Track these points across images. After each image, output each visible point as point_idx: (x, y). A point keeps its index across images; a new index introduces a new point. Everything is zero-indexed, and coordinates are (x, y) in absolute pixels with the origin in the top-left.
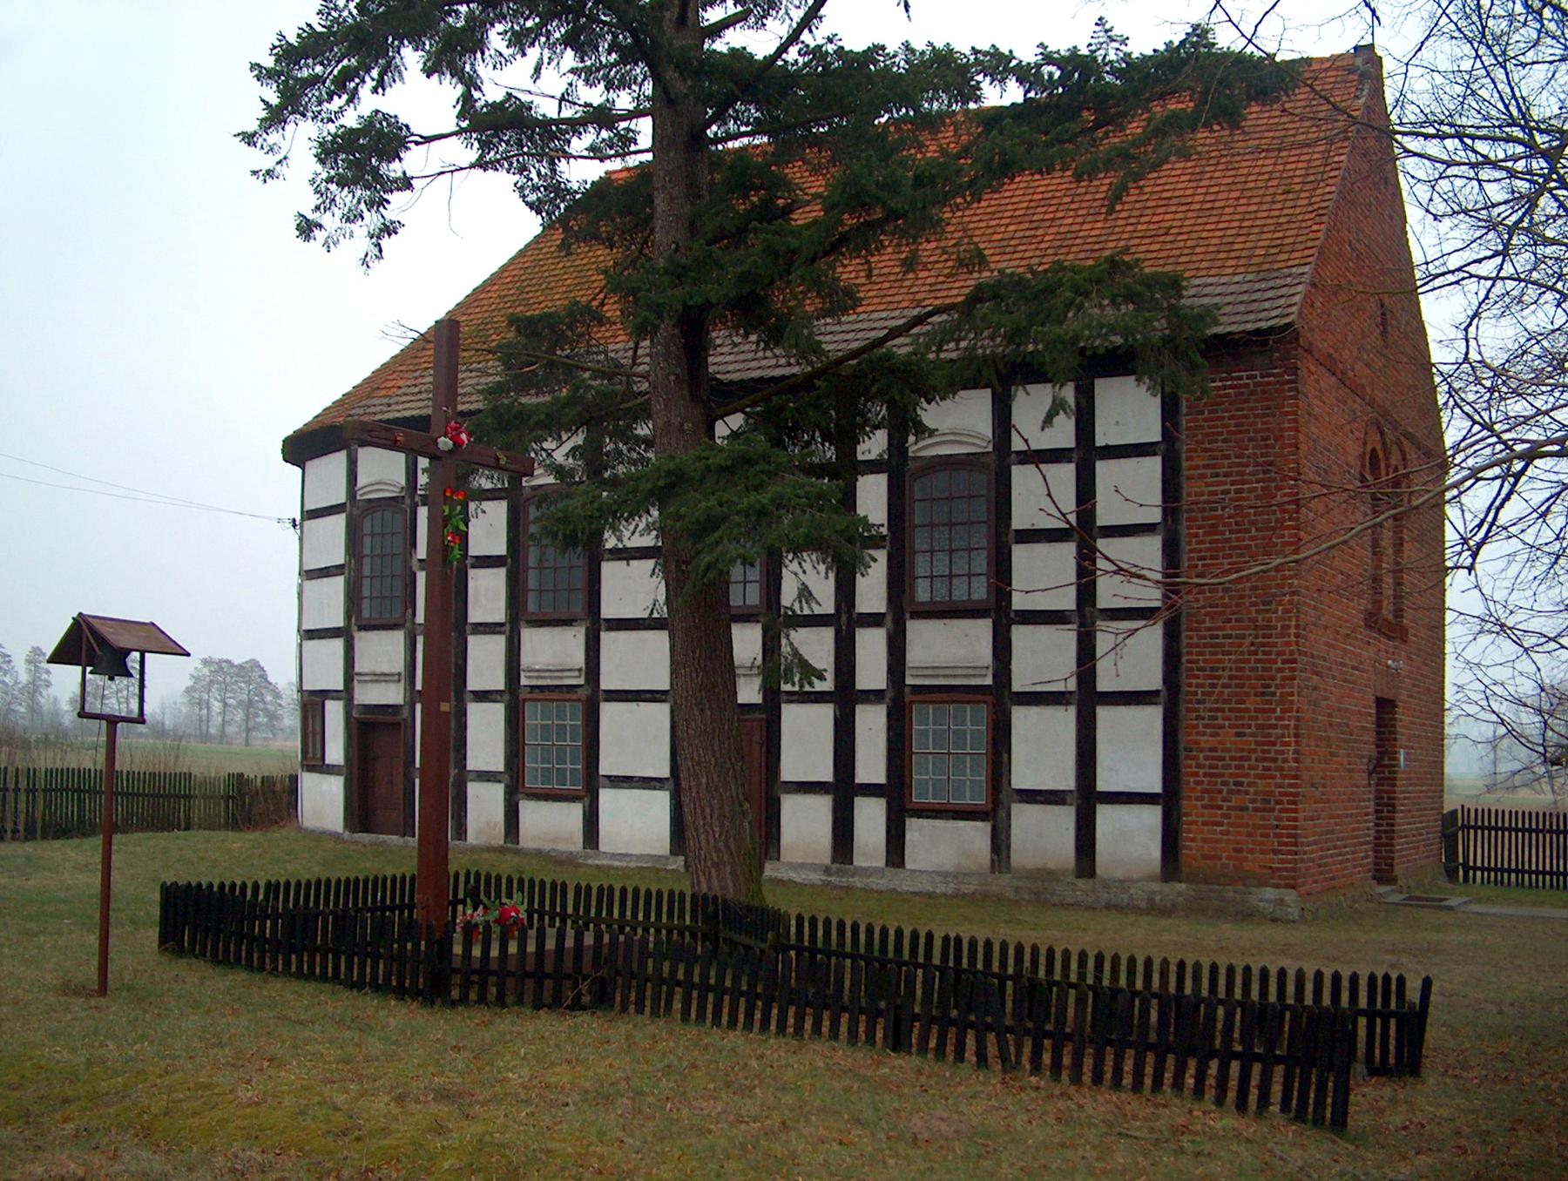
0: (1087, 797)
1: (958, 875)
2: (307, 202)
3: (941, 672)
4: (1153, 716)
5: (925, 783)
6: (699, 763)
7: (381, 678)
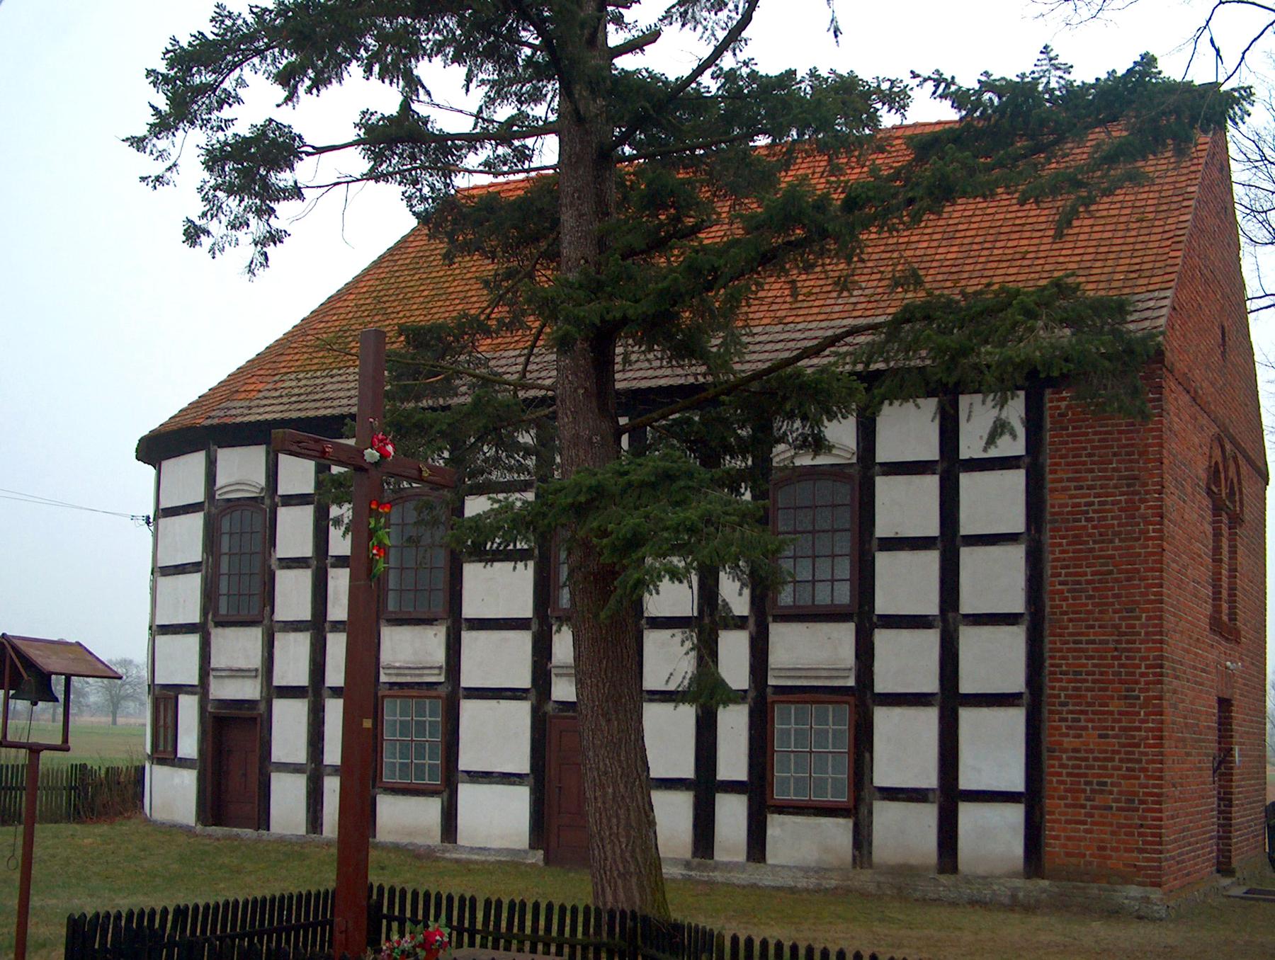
0: (949, 796)
1: (820, 870)
2: (195, 208)
3: (804, 673)
4: (1015, 718)
5: (786, 781)
6: (606, 773)
7: (237, 673)
